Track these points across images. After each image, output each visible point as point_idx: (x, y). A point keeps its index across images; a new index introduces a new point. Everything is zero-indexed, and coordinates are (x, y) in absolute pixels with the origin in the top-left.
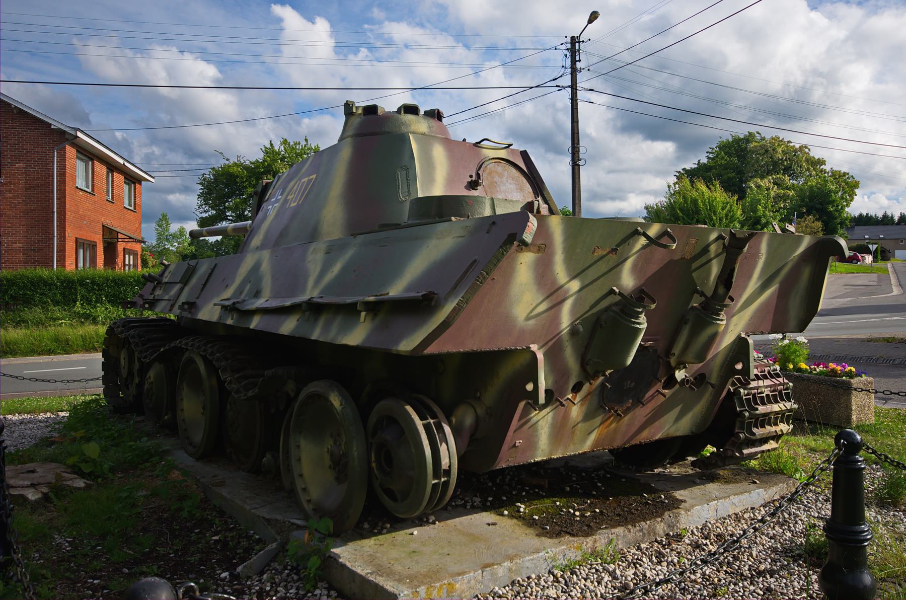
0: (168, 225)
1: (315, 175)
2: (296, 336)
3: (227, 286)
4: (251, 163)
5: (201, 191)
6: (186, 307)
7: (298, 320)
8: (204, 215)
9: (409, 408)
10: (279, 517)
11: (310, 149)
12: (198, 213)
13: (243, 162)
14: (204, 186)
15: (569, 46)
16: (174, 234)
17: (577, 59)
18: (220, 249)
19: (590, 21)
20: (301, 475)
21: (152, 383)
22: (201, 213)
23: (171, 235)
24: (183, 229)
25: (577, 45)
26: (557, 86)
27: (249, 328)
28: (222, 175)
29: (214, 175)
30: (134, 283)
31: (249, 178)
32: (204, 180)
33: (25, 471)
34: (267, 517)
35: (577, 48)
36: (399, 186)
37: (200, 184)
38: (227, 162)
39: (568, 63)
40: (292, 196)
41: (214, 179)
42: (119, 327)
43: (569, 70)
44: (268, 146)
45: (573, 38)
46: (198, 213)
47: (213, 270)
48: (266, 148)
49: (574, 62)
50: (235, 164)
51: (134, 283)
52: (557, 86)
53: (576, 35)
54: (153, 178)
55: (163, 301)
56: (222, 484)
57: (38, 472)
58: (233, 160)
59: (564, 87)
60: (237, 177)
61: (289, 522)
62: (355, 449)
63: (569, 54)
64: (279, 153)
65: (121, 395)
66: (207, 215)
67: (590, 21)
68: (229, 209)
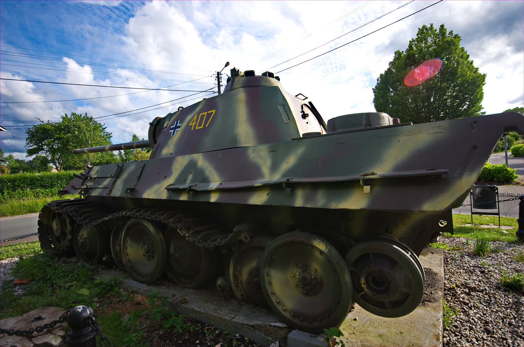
0: (2, 154)
1: (215, 110)
2: (273, 205)
3: (165, 177)
4: (56, 123)
5: (28, 137)
6: (129, 191)
7: (268, 195)
8: (30, 148)
9: (394, 246)
10: (259, 323)
11: (87, 118)
12: (27, 147)
13: (51, 123)
14: (30, 134)
15: (217, 76)
16: (6, 158)
17: (220, 81)
18: (32, 164)
19: (226, 66)
20: (273, 294)
21: (86, 238)
22: (29, 147)
23: (4, 158)
24: (11, 155)
25: (220, 75)
26: (213, 92)
27: (209, 202)
28: (40, 129)
29: (35, 129)
30: (7, 182)
31: (55, 131)
32: (29, 131)
33: (32, 319)
34: (251, 324)
35: (220, 77)
36: (281, 114)
37: (27, 133)
38: (42, 123)
39: (217, 82)
40: (195, 123)
41: (35, 131)
42: (54, 206)
43: (217, 85)
44: (64, 116)
45: (218, 73)
46: (27, 147)
47: (143, 168)
48: (63, 117)
49: (219, 82)
50: (47, 124)
51: (7, 182)
52: (213, 92)
53: (219, 71)
54: (5, 129)
55: (98, 189)
56: (185, 301)
57: (44, 318)
58: (46, 122)
59: (216, 92)
60: (49, 130)
61: (271, 326)
62: (347, 277)
63: (217, 79)
64: (71, 119)
65: (53, 247)
66: (32, 148)
67: (226, 66)
68: (45, 145)
